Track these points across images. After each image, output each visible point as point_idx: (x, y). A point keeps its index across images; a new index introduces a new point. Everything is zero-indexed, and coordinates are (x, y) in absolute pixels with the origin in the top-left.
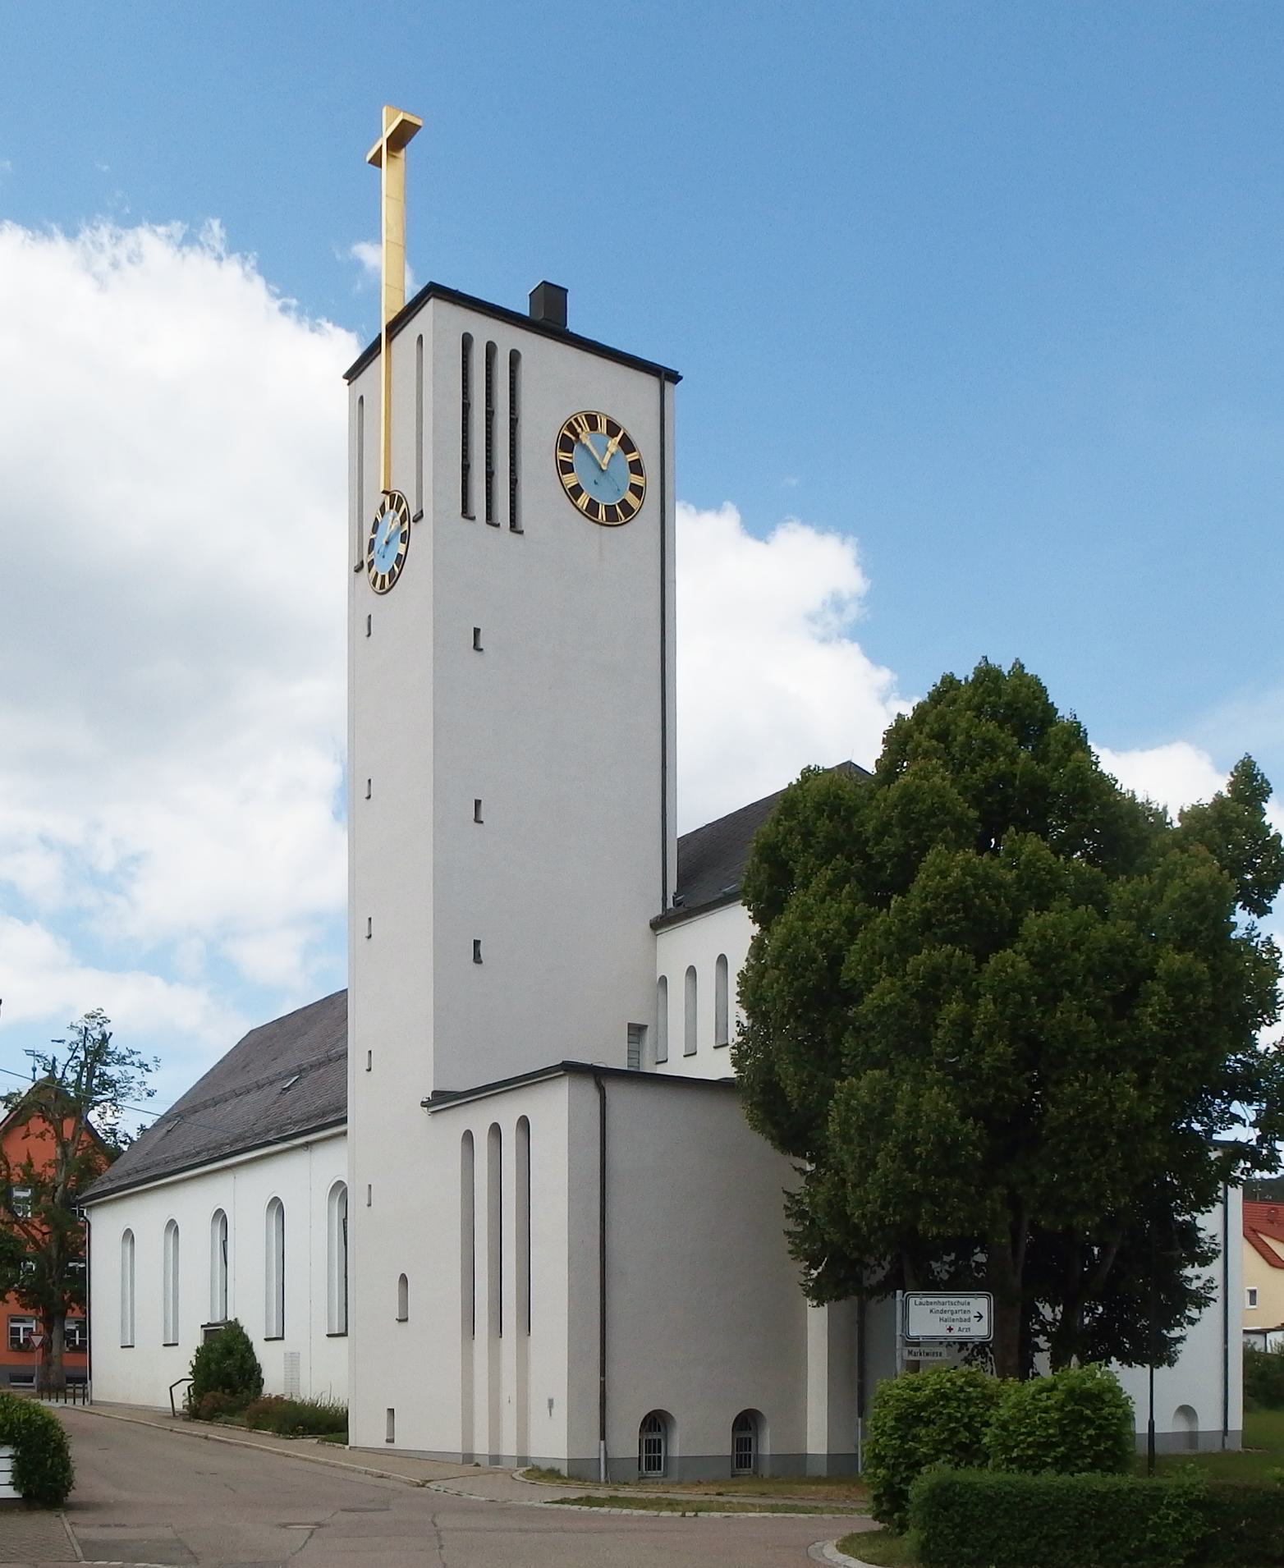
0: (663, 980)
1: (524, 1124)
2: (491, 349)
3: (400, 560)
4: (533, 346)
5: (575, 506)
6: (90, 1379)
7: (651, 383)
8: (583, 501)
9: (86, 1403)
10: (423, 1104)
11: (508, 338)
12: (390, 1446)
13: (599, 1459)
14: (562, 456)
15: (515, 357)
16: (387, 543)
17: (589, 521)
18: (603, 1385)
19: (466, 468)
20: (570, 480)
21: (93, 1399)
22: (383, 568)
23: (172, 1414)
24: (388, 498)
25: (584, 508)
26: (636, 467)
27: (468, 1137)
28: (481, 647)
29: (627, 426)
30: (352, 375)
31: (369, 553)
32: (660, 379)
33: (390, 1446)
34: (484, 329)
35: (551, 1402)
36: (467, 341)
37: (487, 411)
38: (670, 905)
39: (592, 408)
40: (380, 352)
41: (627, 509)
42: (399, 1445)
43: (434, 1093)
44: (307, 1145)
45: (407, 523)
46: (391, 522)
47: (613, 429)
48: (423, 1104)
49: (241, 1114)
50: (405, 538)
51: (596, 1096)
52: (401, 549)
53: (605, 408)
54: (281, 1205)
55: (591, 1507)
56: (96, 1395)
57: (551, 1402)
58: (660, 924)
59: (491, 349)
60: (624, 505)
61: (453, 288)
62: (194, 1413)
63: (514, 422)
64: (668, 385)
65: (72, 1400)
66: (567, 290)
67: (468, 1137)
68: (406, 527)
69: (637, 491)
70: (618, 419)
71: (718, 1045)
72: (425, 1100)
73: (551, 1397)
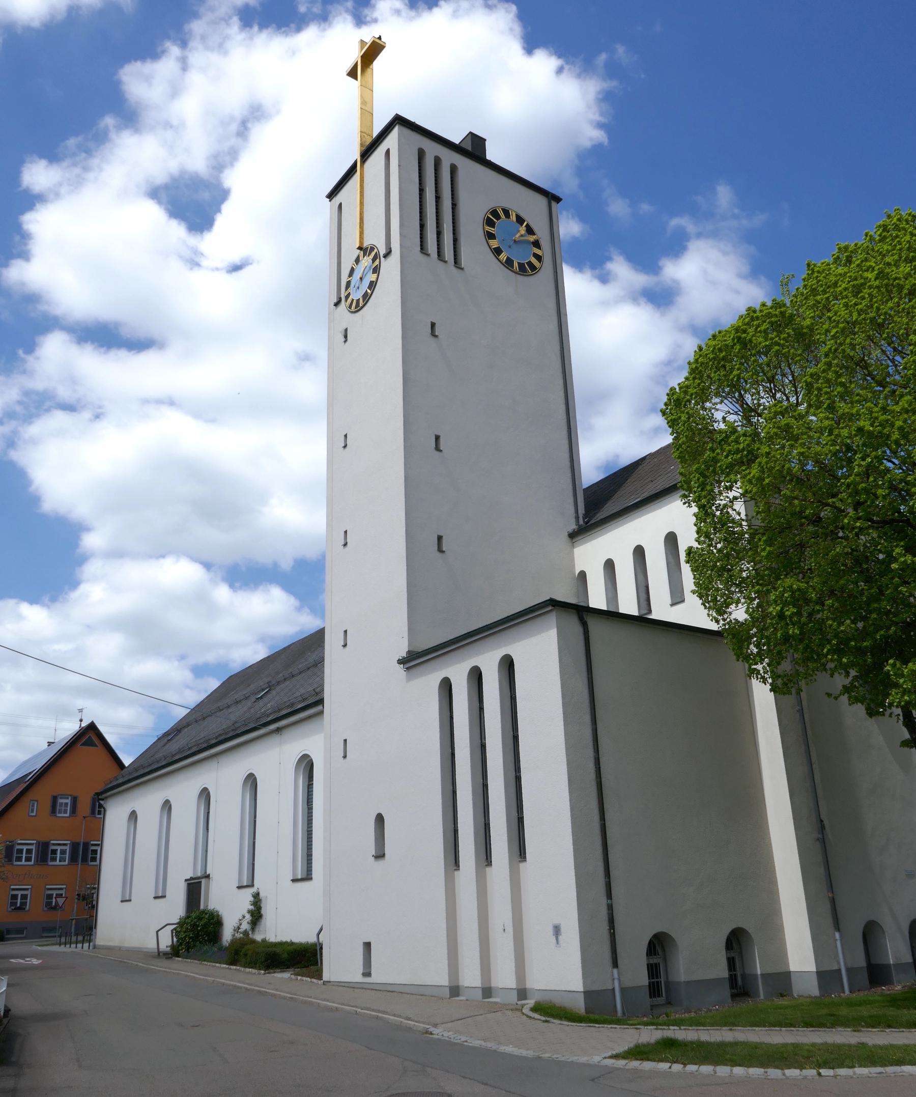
0: (583, 575)
1: (508, 666)
2: (437, 162)
3: (372, 285)
4: (465, 166)
5: (498, 259)
6: (95, 928)
7: (542, 201)
8: (503, 257)
9: (91, 948)
10: (401, 662)
11: (449, 158)
12: (367, 980)
13: (614, 989)
14: (488, 228)
15: (454, 169)
16: (361, 279)
17: (507, 270)
18: (610, 908)
19: (422, 226)
20: (494, 244)
21: (97, 943)
22: (357, 295)
23: (157, 954)
24: (362, 253)
25: (504, 261)
26: (537, 244)
27: (446, 687)
28: (437, 334)
29: (529, 219)
30: (331, 195)
31: (346, 290)
32: (548, 199)
33: (367, 980)
34: (433, 150)
35: (557, 930)
36: (421, 154)
37: (436, 196)
38: (581, 522)
39: (507, 205)
40: (356, 171)
41: (533, 268)
42: (378, 977)
43: (409, 652)
44: (278, 730)
45: (378, 260)
46: (366, 261)
47: (520, 220)
48: (401, 662)
49: (214, 726)
50: (376, 270)
51: (175, 922)
52: (373, 277)
53: (516, 208)
54: (255, 780)
55: (685, 1065)
56: (326, 976)
57: (557, 930)
58: (575, 536)
59: (437, 162)
60: (530, 264)
61: (413, 120)
62: (175, 952)
63: (454, 206)
64: (554, 204)
65: (81, 945)
66: (485, 140)
67: (446, 687)
68: (377, 262)
69: (539, 258)
70: (523, 215)
71: (674, 602)
72: (401, 658)
73: (556, 922)
